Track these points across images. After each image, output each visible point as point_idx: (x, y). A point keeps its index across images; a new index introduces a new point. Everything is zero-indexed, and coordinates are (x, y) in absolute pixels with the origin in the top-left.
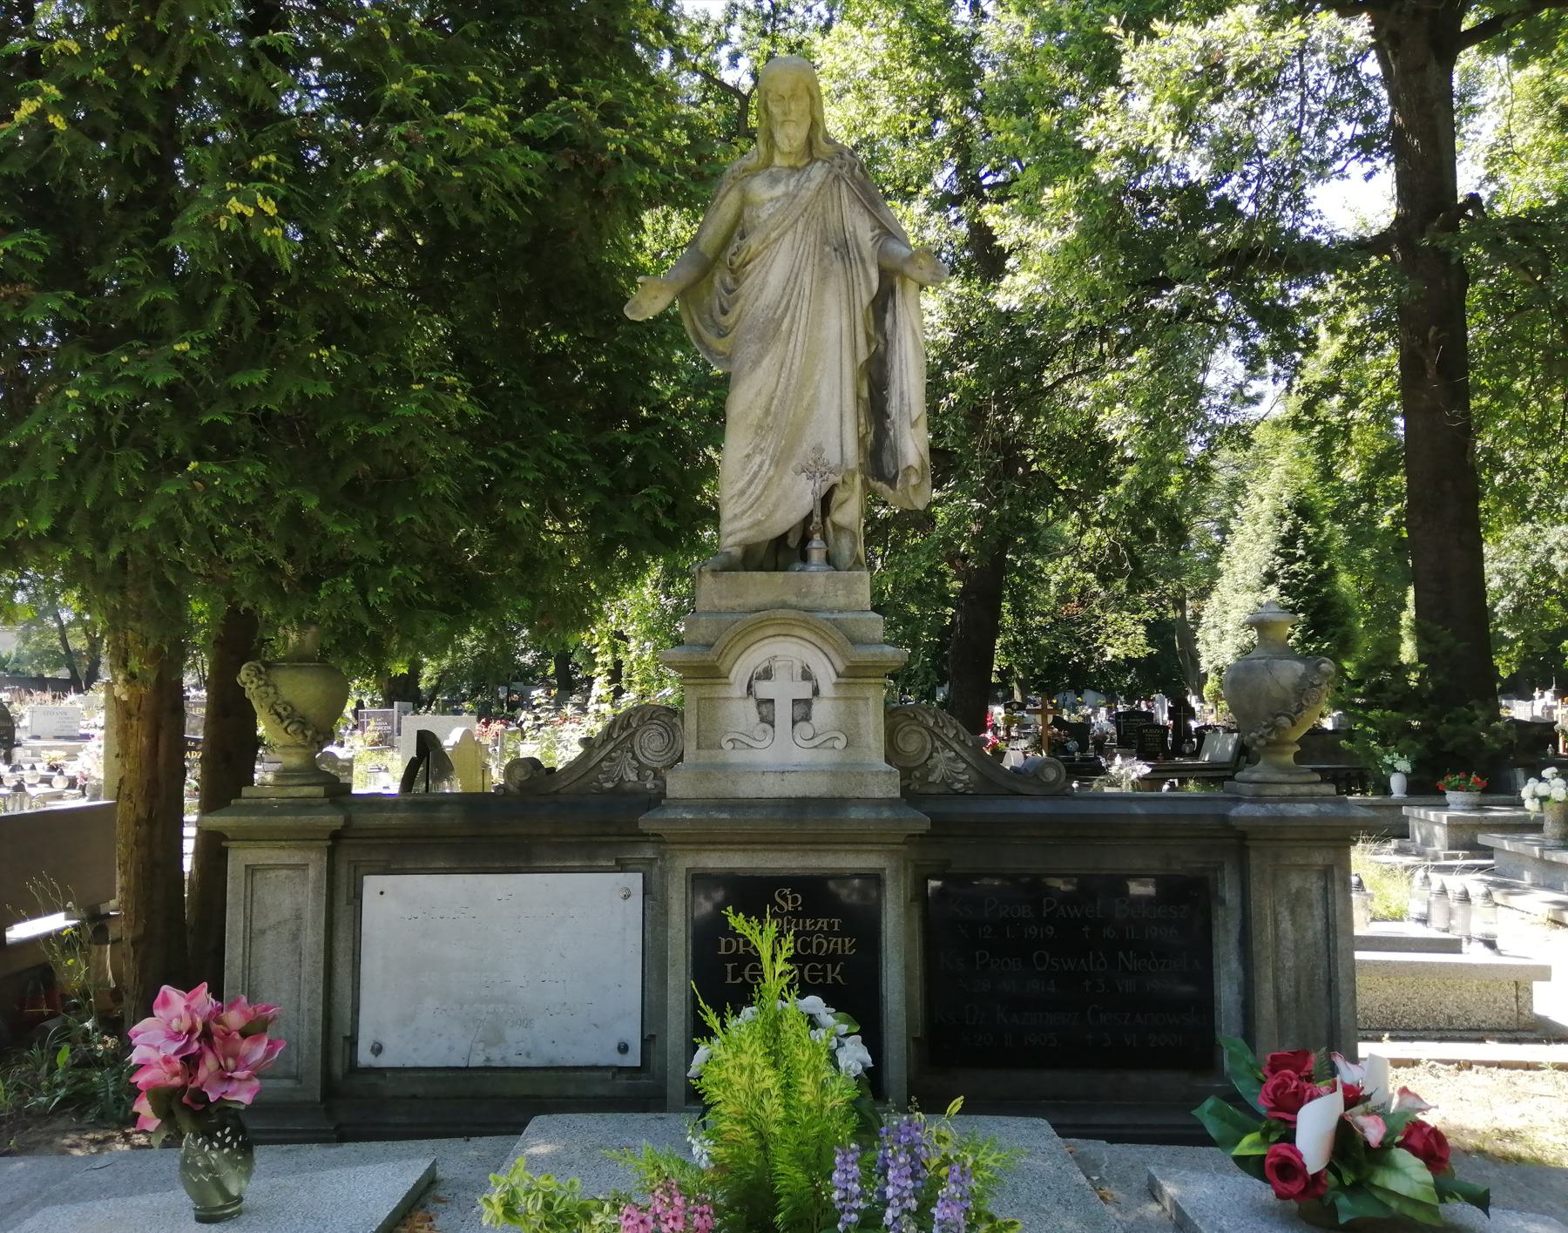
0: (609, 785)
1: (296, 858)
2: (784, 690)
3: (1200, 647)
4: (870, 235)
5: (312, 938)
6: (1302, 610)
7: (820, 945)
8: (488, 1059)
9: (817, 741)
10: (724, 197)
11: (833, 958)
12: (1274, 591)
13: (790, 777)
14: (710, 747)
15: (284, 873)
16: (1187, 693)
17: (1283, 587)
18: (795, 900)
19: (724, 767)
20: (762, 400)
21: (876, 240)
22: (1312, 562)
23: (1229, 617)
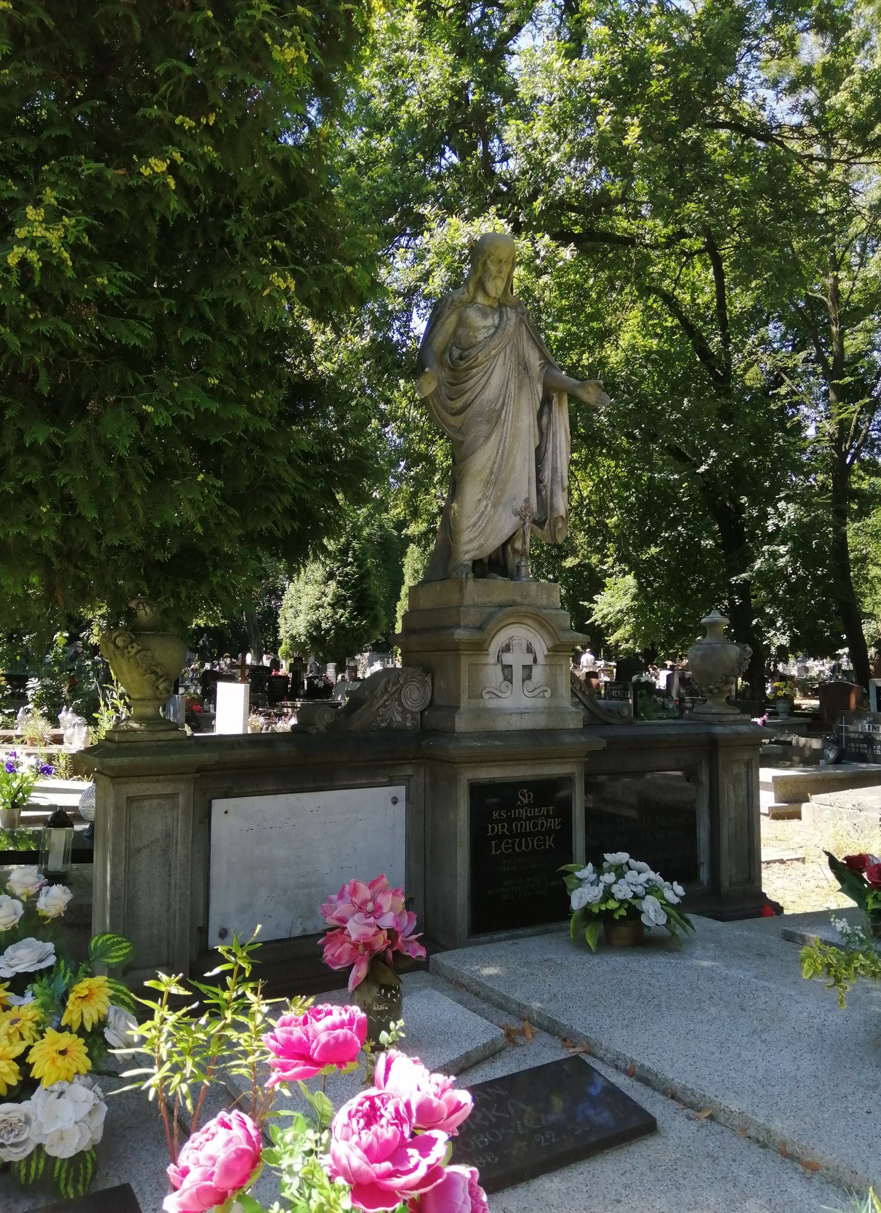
0: (384, 725)
1: (169, 790)
2: (517, 659)
3: (281, 621)
4: (539, 362)
5: (181, 851)
6: (350, 598)
7: (542, 824)
8: (304, 930)
9: (535, 693)
10: (448, 317)
11: (549, 832)
12: (333, 584)
13: (525, 716)
14: (475, 697)
15: (156, 801)
16: (249, 651)
17: (339, 582)
18: (529, 796)
19: (488, 711)
20: (490, 464)
21: (542, 367)
22: (358, 567)
23: (302, 601)
